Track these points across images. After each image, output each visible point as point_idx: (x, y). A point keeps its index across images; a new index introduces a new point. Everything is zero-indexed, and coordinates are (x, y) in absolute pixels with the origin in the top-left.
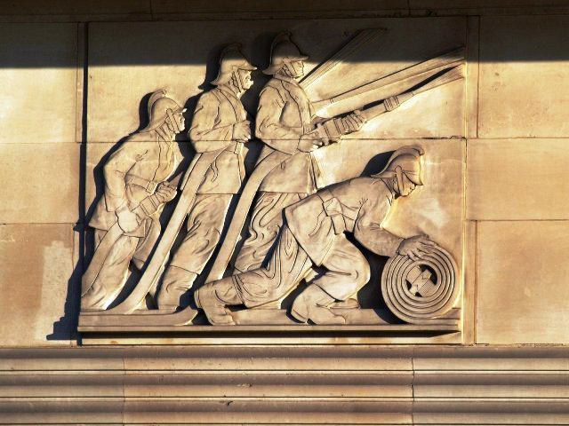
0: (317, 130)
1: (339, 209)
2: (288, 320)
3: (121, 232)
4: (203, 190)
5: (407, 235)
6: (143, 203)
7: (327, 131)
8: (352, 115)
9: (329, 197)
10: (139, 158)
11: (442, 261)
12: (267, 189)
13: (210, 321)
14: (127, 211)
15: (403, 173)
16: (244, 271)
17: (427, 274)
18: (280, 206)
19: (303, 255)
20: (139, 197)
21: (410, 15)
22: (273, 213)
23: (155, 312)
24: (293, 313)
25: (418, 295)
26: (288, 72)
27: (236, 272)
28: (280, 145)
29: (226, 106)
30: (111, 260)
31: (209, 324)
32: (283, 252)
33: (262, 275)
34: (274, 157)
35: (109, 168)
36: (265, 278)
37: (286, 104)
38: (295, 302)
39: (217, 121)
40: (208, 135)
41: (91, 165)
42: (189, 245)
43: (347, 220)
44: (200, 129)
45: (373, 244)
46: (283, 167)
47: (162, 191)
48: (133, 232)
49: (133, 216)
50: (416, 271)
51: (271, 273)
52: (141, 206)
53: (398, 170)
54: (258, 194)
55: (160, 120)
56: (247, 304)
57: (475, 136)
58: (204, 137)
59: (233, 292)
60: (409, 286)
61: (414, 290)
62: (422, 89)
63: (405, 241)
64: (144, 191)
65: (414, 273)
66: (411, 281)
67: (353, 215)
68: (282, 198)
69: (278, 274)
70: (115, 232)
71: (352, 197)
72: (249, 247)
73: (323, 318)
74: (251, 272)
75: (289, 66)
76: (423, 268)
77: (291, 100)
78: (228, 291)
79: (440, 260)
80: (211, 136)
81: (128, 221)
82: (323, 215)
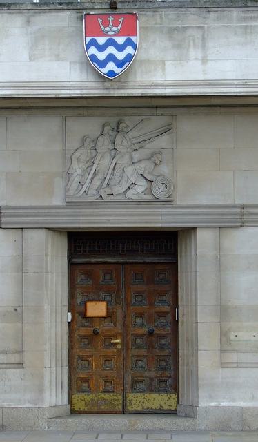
12: (119, 162)
18: (122, 167)
41: (68, 156)
45: (149, 178)
71: (143, 165)
78: (109, 191)
81: (79, 171)
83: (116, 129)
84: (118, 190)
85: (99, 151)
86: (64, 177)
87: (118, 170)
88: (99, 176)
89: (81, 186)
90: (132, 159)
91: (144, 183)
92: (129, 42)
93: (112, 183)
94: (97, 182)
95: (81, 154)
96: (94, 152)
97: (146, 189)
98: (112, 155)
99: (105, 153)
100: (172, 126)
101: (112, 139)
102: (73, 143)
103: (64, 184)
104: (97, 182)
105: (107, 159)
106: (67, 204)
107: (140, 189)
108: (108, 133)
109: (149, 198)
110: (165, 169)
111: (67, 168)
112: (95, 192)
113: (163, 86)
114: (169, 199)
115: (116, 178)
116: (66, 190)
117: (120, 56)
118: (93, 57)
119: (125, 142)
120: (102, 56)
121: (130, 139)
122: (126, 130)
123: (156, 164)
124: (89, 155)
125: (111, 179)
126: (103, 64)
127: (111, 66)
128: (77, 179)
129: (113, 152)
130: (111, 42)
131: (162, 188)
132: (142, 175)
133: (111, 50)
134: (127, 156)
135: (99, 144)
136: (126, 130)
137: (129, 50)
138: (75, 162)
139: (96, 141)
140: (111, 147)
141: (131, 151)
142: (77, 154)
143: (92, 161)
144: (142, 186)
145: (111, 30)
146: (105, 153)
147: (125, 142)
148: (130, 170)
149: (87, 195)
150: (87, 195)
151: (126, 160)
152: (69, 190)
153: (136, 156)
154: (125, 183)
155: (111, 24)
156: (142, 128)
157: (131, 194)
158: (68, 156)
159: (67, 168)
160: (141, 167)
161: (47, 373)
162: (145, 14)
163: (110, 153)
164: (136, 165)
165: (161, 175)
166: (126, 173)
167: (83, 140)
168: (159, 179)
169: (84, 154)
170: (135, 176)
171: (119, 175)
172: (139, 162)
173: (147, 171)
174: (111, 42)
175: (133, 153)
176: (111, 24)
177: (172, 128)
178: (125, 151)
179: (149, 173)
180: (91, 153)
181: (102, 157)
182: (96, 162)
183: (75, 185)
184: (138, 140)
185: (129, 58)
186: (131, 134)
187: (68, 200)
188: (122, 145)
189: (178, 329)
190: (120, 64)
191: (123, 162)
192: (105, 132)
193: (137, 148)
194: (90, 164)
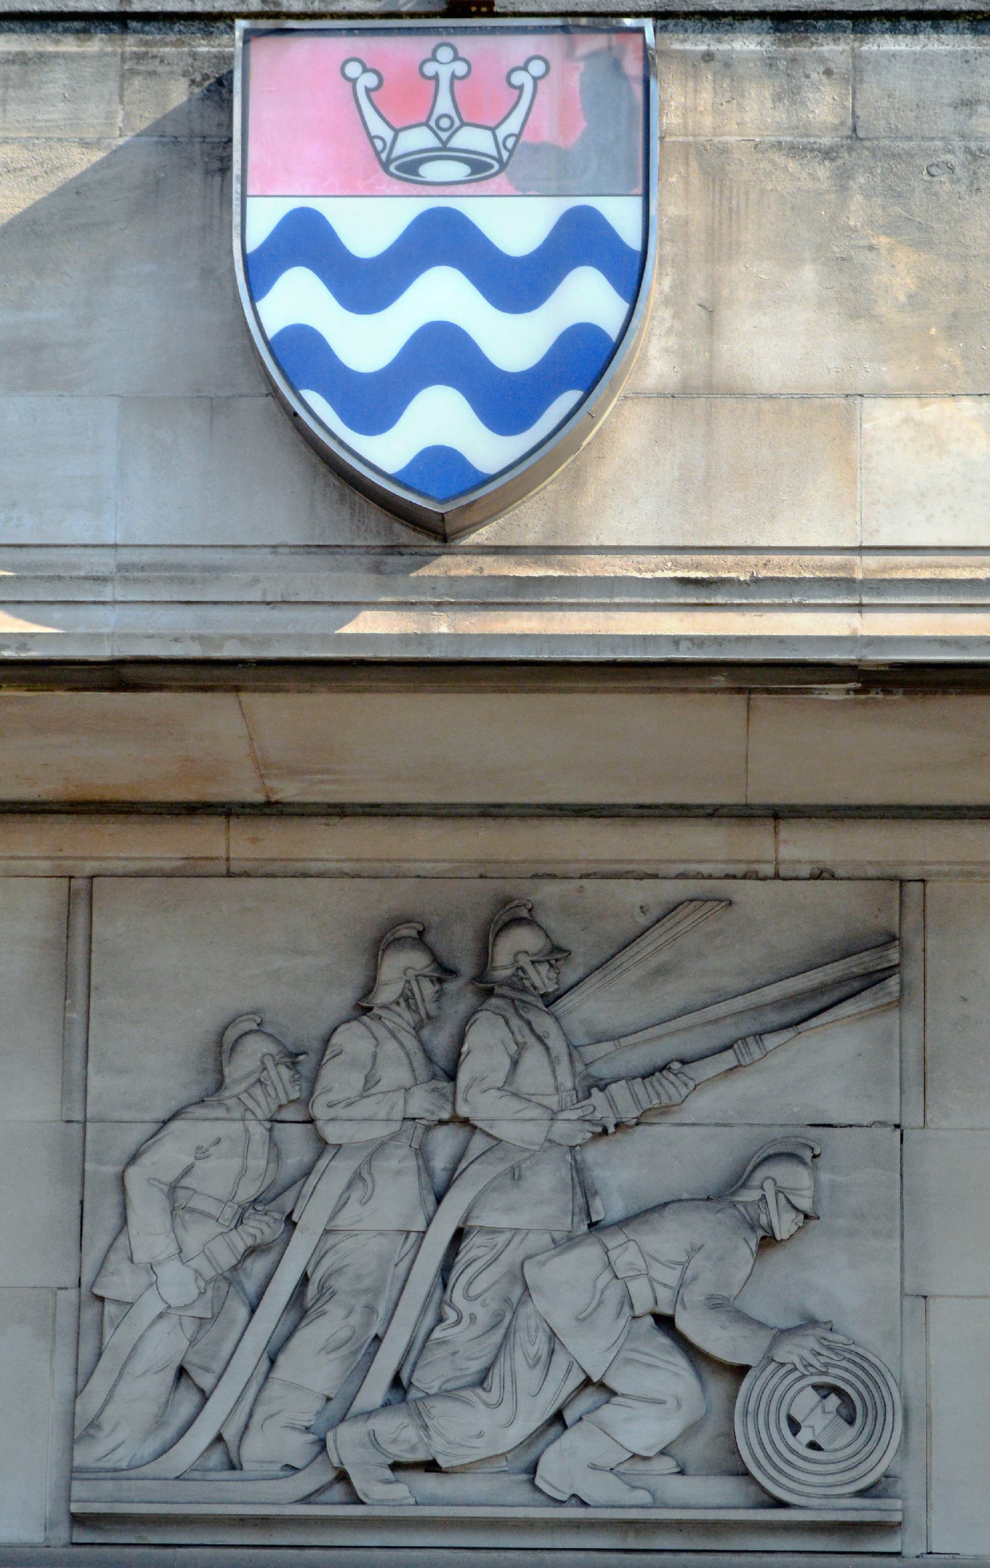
0: (592, 1100)
1: (641, 1264)
2: (524, 1493)
3: (161, 1307)
4: (342, 1221)
5: (784, 1324)
6: (211, 1245)
7: (611, 1103)
8: (664, 1072)
9: (621, 1238)
10: (202, 1153)
11: (880, 1411)
12: (486, 1218)
13: (362, 1497)
14: (175, 1265)
15: (778, 1192)
16: (432, 1392)
17: (834, 1400)
18: (512, 1256)
19: (560, 1360)
20: (196, 1235)
21: (777, 876)
22: (496, 1271)
23: (236, 1474)
24: (538, 1481)
25: (813, 1446)
26: (527, 983)
27: (413, 1394)
28: (504, 1130)
29: (390, 1046)
30: (138, 1366)
31: (253, 300)
32: (519, 1356)
33: (475, 1399)
34: (499, 1154)
35: (135, 1176)
36: (482, 1407)
37: (521, 1047)
38: (307, 270)
39: (370, 1083)
40: (351, 1108)
41: (102, 1170)
42: (314, 1334)
43: (659, 1288)
44: (331, 1097)
45: (719, 1340)
46: (515, 1175)
47: (252, 1223)
48: (186, 1307)
49: (188, 1275)
50: (811, 1397)
51: (493, 1397)
52: (204, 1251)
53: (768, 1185)
54: (459, 1235)
55: (248, 1076)
56: (442, 1462)
57: (922, 1124)
58: (339, 1112)
59: (411, 1433)
60: (795, 1427)
61: (805, 1435)
62: (814, 1022)
63: (783, 1333)
64: (213, 1222)
65: (805, 1403)
66: (799, 1418)
67: (671, 1276)
68: (517, 1239)
69: (508, 1396)
70: (150, 1306)
71: (667, 1240)
72: (442, 1342)
73: (605, 1492)
74: (446, 1394)
75: (530, 969)
76: (825, 1390)
77: (531, 1040)
78: (400, 1434)
79: (861, 1373)
80: (360, 1110)
81: (178, 1284)
82: (607, 1276)
83: (467, 967)
84: (471, 1429)
85: (332, 1133)
86: (66, 1320)
87: (479, 1281)
88: (329, 1326)
89: (186, 1402)
90: (583, 1187)
91: (673, 1378)
92: (580, 240)
93: (427, 1379)
94: (313, 1366)
95: (202, 1153)
96: (296, 1142)
97: (691, 1430)
98: (440, 1162)
99: (379, 1148)
100: (894, 956)
101: (441, 1041)
102: (144, 1062)
103: (65, 1383)
104: (313, 1366)
105: (395, 1195)
106: (82, 1536)
107: (643, 1429)
108: (407, 998)
109: (709, 1495)
110: (838, 1280)
111: (92, 1256)
112: (296, 1447)
113: (848, 584)
114: (868, 1511)
115: (464, 1346)
116: (78, 1431)
117: (514, 341)
118: (303, 352)
119: (534, 1058)
120: (367, 342)
121: (573, 1048)
122: (542, 978)
123: (768, 1241)
124: (258, 1162)
125: (419, 1348)
126: (377, 400)
127: (439, 419)
128: (165, 1346)
129: (444, 1145)
130: (442, 239)
131: (819, 1419)
132: (665, 1322)
133: (442, 295)
134: (548, 1178)
135: (339, 1080)
136: (542, 978)
137: (586, 297)
138: (147, 1212)
139: (303, 1060)
140: (422, 1103)
141: (581, 1134)
142: (171, 1154)
143: (275, 1205)
144: (658, 1403)
145: (444, 152)
146: (379, 1148)
147: (534, 1058)
148: (567, 1282)
149: (233, 1465)
150: (233, 1465)
151: (539, 1204)
152: (94, 1424)
153: (621, 1174)
154: (528, 1378)
155: (444, 105)
156: (662, 972)
157: (564, 1465)
158: (102, 1170)
159: (92, 1256)
160: (660, 1259)
161: (885, 47)
162: (708, 57)
163: (422, 1153)
164: (613, 1240)
165: (811, 1322)
166: (539, 1303)
167: (222, 1048)
168: (789, 1352)
169: (223, 1155)
170: (610, 1326)
171: (484, 1316)
172: (642, 1215)
173: (696, 1294)
174: (442, 239)
175: (593, 1155)
176: (444, 105)
177: (891, 970)
178: (533, 1133)
179: (716, 1304)
180: (275, 1151)
181: (358, 1176)
182: (313, 1217)
183: (145, 1388)
184: (640, 1056)
185: (586, 361)
186: (590, 1008)
187: (90, 1497)
188: (509, 1087)
189: (11, 634)
190: (505, 400)
191: (521, 1220)
192: (386, 994)
193: (630, 1113)
194: (261, 1227)
